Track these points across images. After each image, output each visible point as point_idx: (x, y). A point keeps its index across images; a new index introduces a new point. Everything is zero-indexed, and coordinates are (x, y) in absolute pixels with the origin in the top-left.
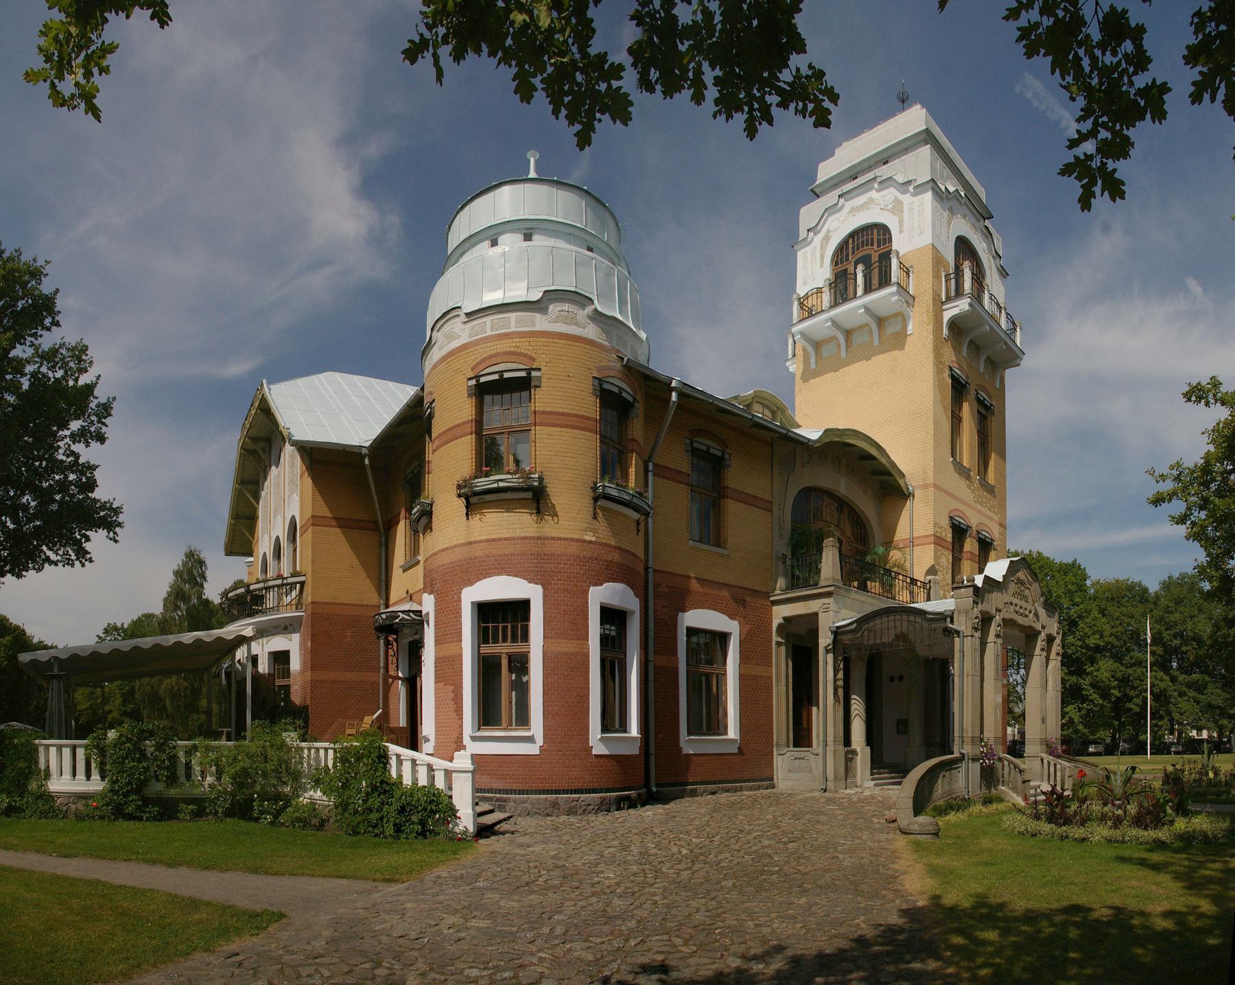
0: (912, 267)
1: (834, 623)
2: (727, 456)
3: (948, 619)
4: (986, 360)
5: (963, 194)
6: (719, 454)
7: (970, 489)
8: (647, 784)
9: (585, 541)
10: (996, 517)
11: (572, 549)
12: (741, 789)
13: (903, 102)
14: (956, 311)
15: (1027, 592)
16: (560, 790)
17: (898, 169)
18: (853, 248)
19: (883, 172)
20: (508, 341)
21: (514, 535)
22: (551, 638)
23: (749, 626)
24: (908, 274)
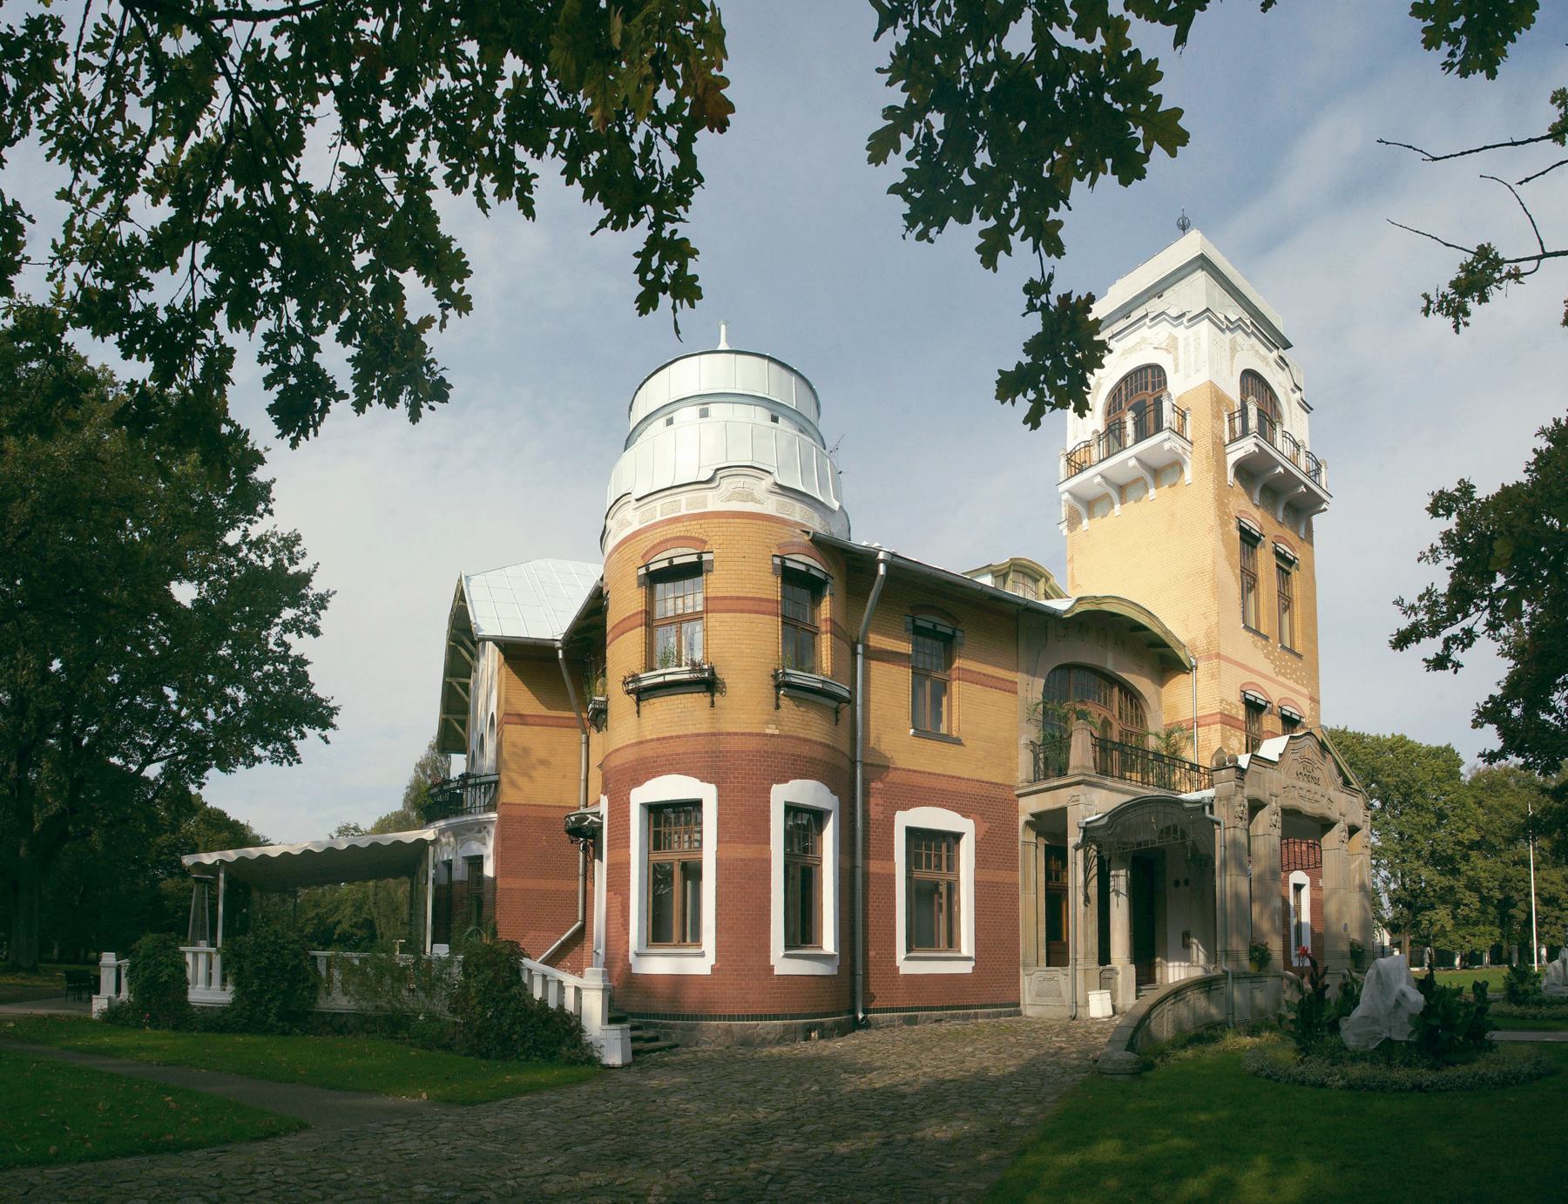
0: (1188, 409)
1: (1084, 818)
2: (958, 634)
3: (1207, 808)
4: (1285, 508)
5: (1248, 322)
6: (949, 631)
7: (1269, 658)
8: (853, 1011)
9: (766, 735)
10: (1305, 691)
11: (752, 744)
12: (976, 1016)
13: (1184, 229)
14: (1240, 454)
15: (1317, 774)
16: (734, 1016)
17: (1172, 301)
18: (1126, 394)
19: (1154, 306)
20: (678, 525)
21: (686, 732)
22: (727, 842)
23: (988, 825)
24: (1184, 417)
